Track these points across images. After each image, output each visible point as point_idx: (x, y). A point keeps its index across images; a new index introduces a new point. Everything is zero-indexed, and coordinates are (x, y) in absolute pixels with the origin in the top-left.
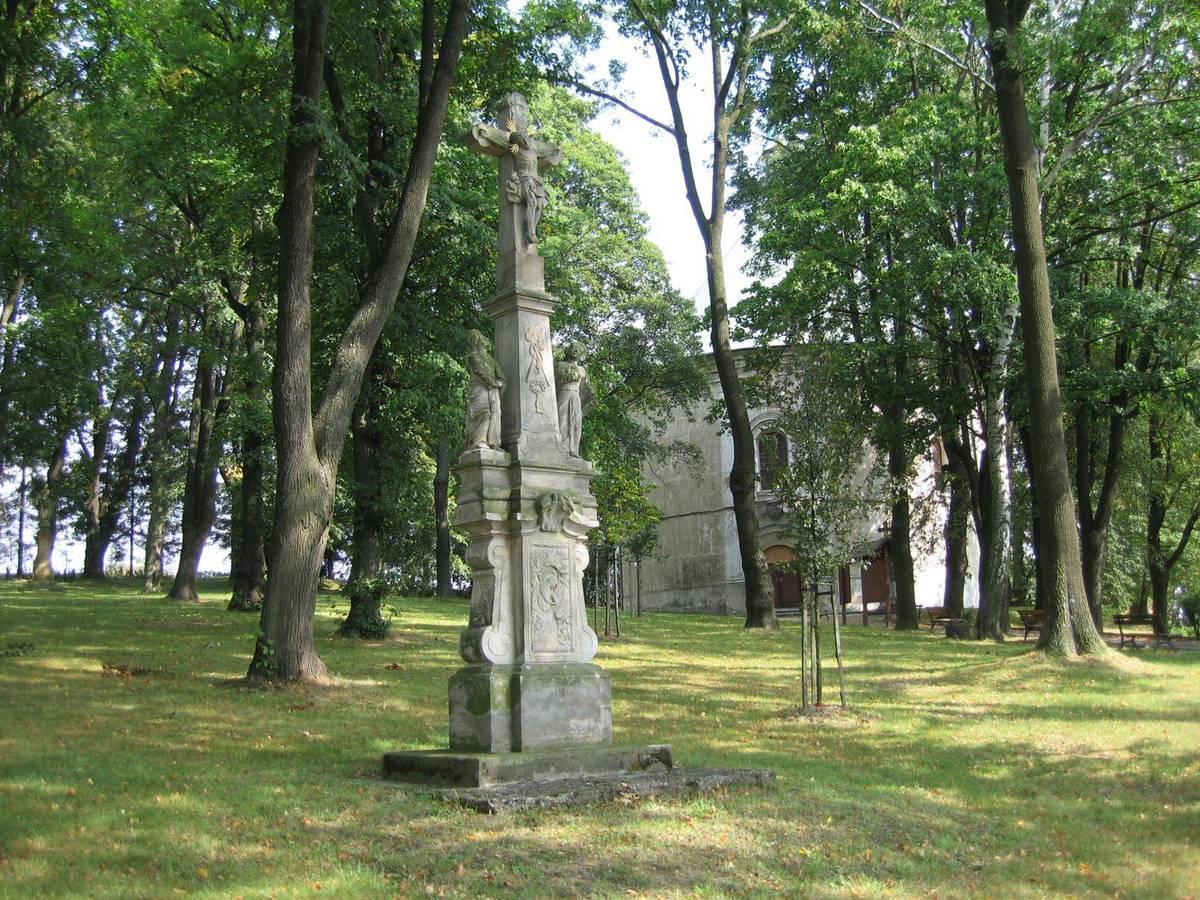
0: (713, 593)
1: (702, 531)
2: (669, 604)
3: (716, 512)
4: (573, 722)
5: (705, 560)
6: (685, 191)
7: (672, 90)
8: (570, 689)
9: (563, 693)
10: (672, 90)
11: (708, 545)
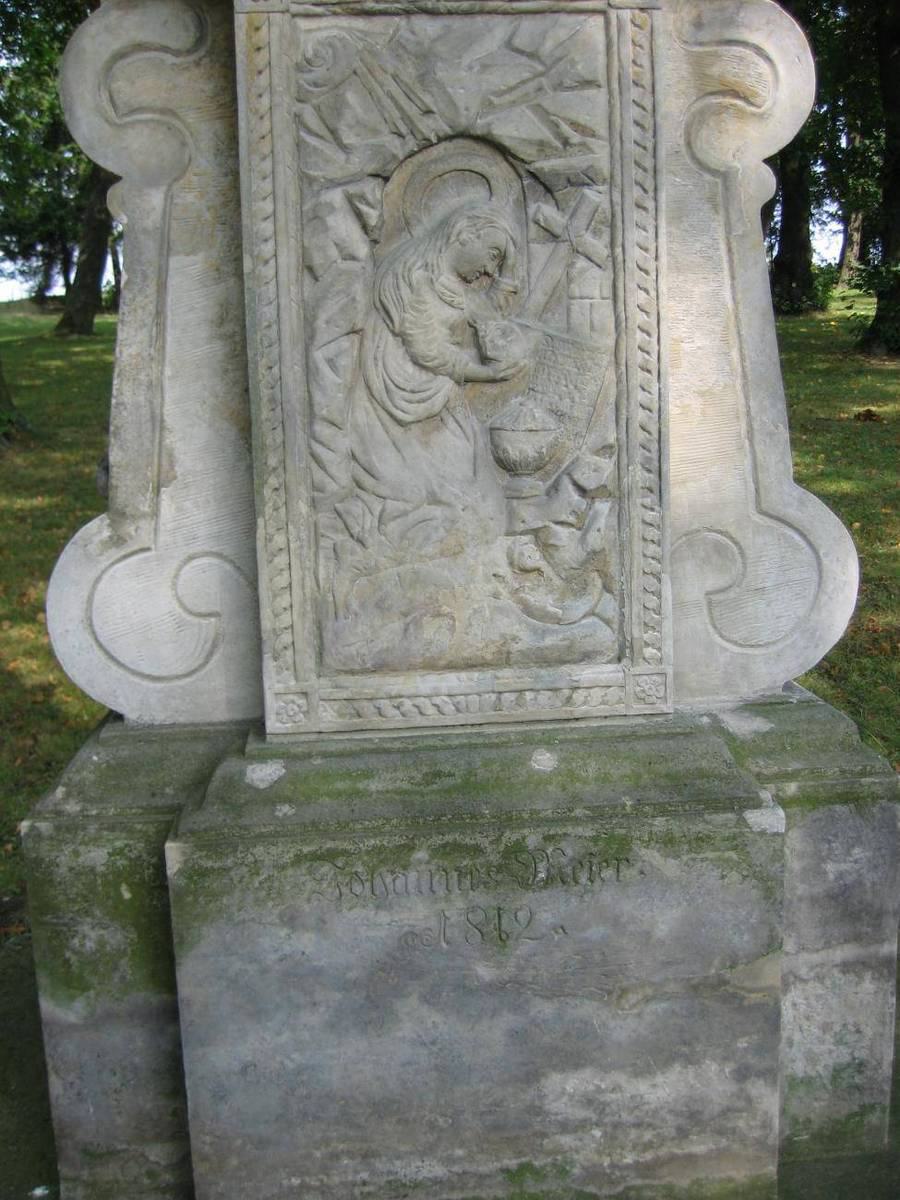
4: (564, 1090)
8: (548, 908)
9: (496, 936)
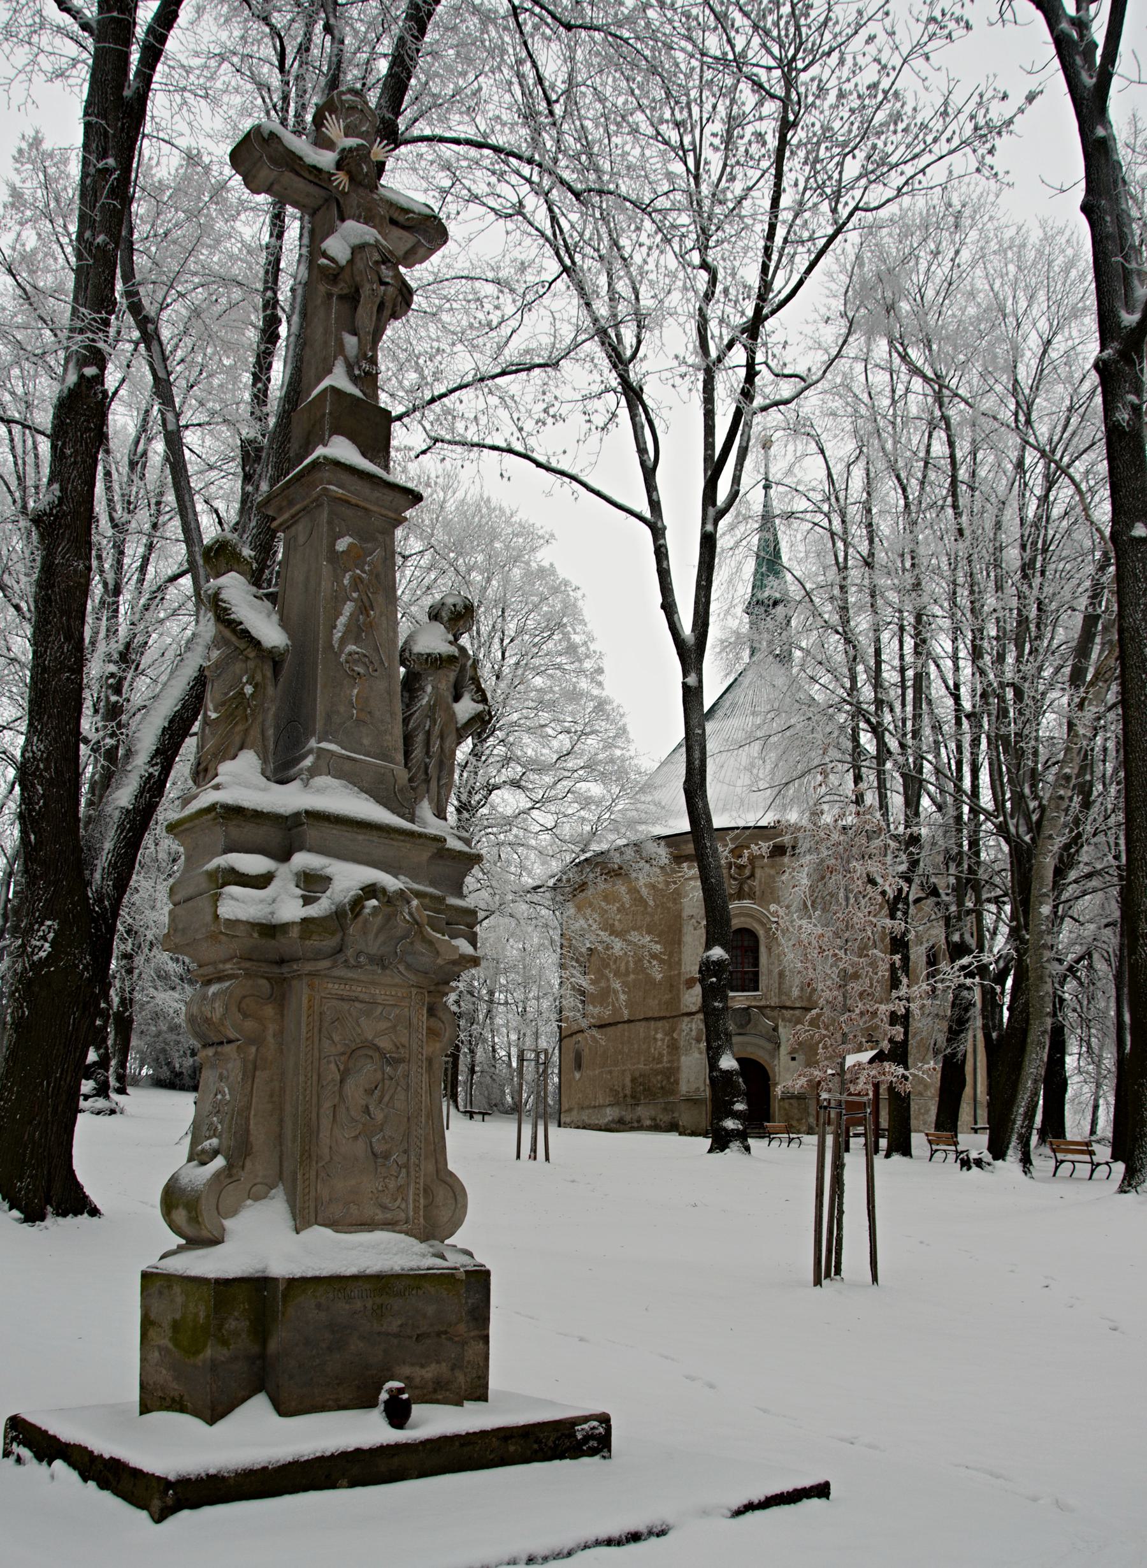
0: (665, 1109)
1: (655, 1039)
2: (613, 1121)
3: (673, 1016)
5: (657, 1072)
6: (659, 599)
7: (649, 474)
10: (649, 474)
11: (661, 1055)
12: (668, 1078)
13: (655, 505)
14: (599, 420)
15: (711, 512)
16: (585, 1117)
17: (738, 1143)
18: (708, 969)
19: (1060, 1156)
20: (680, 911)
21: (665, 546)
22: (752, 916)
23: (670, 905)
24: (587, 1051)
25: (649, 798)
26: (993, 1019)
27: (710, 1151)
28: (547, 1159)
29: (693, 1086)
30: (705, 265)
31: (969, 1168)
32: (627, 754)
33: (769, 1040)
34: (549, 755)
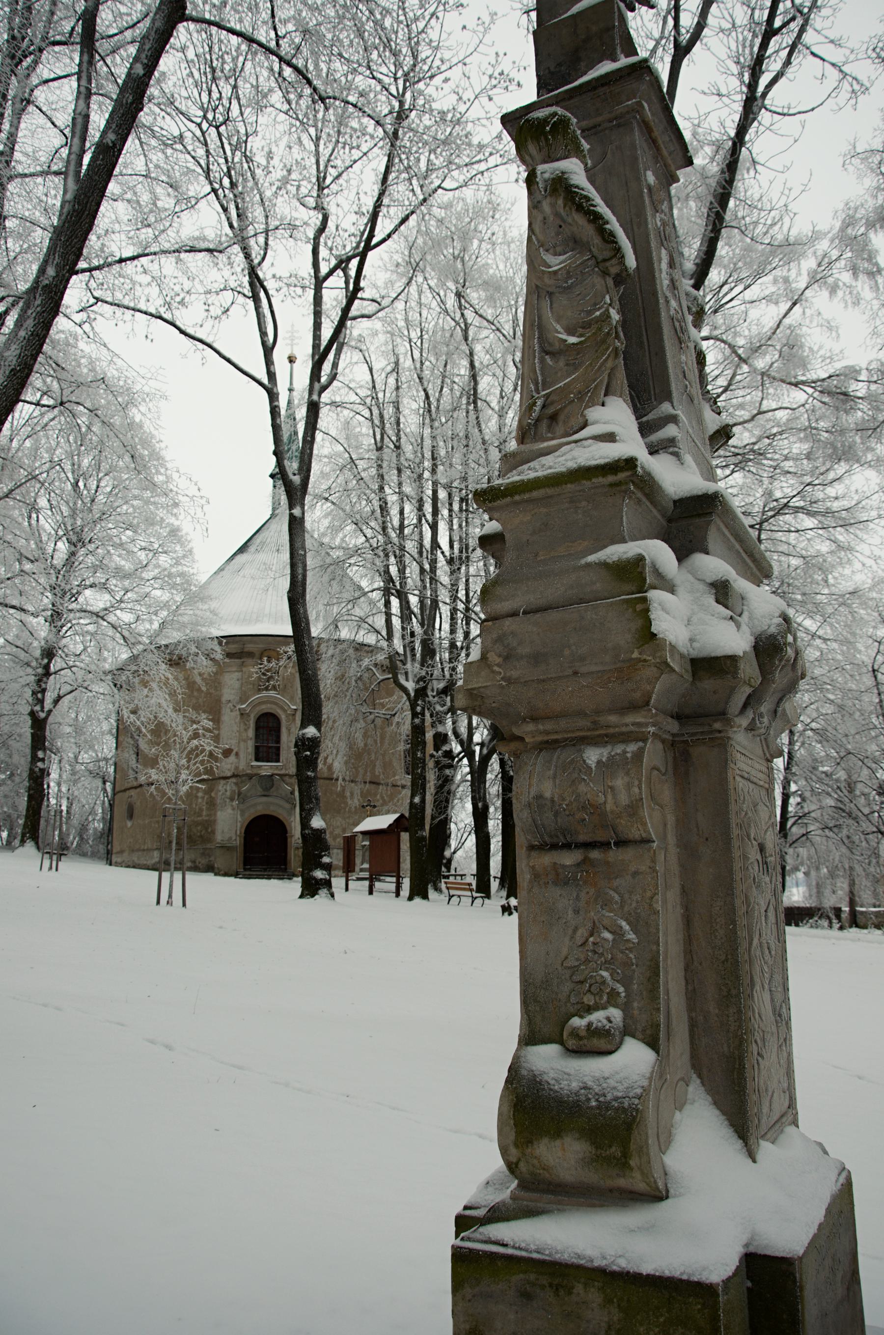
0: (203, 854)
1: (197, 797)
5: (197, 824)
7: (268, 351)
10: (268, 351)
11: (201, 810)
12: (206, 829)
13: (271, 375)
14: (216, 311)
15: (317, 386)
16: (135, 858)
17: (325, 890)
18: (303, 744)
19: (452, 892)
20: (220, 696)
21: (278, 407)
22: (260, 704)
23: (212, 691)
24: (138, 803)
25: (206, 607)
26: (479, 793)
27: (301, 897)
28: (184, 905)
29: (227, 836)
30: (319, 207)
31: (510, 914)
32: (192, 571)
33: (287, 801)
34: (127, 566)
